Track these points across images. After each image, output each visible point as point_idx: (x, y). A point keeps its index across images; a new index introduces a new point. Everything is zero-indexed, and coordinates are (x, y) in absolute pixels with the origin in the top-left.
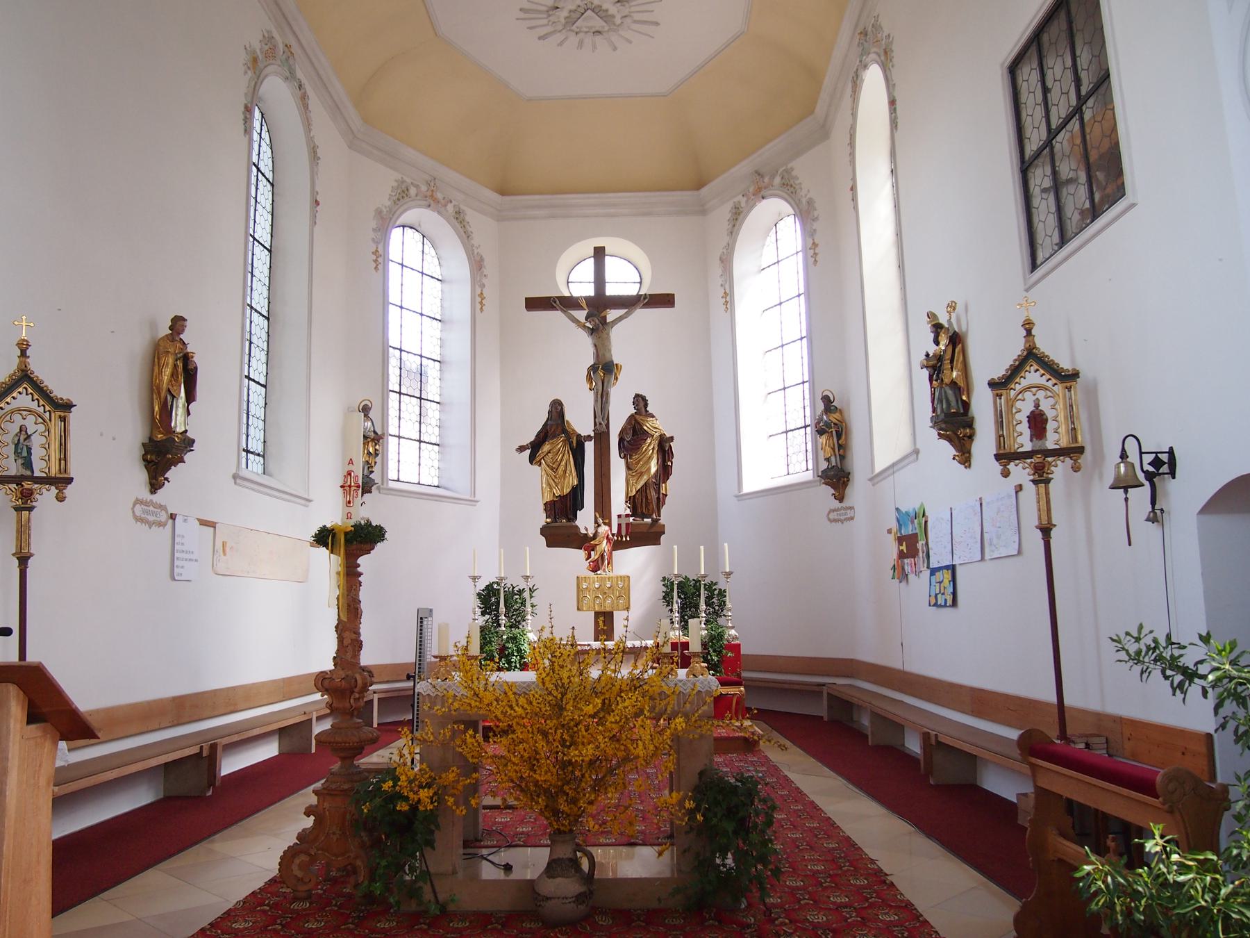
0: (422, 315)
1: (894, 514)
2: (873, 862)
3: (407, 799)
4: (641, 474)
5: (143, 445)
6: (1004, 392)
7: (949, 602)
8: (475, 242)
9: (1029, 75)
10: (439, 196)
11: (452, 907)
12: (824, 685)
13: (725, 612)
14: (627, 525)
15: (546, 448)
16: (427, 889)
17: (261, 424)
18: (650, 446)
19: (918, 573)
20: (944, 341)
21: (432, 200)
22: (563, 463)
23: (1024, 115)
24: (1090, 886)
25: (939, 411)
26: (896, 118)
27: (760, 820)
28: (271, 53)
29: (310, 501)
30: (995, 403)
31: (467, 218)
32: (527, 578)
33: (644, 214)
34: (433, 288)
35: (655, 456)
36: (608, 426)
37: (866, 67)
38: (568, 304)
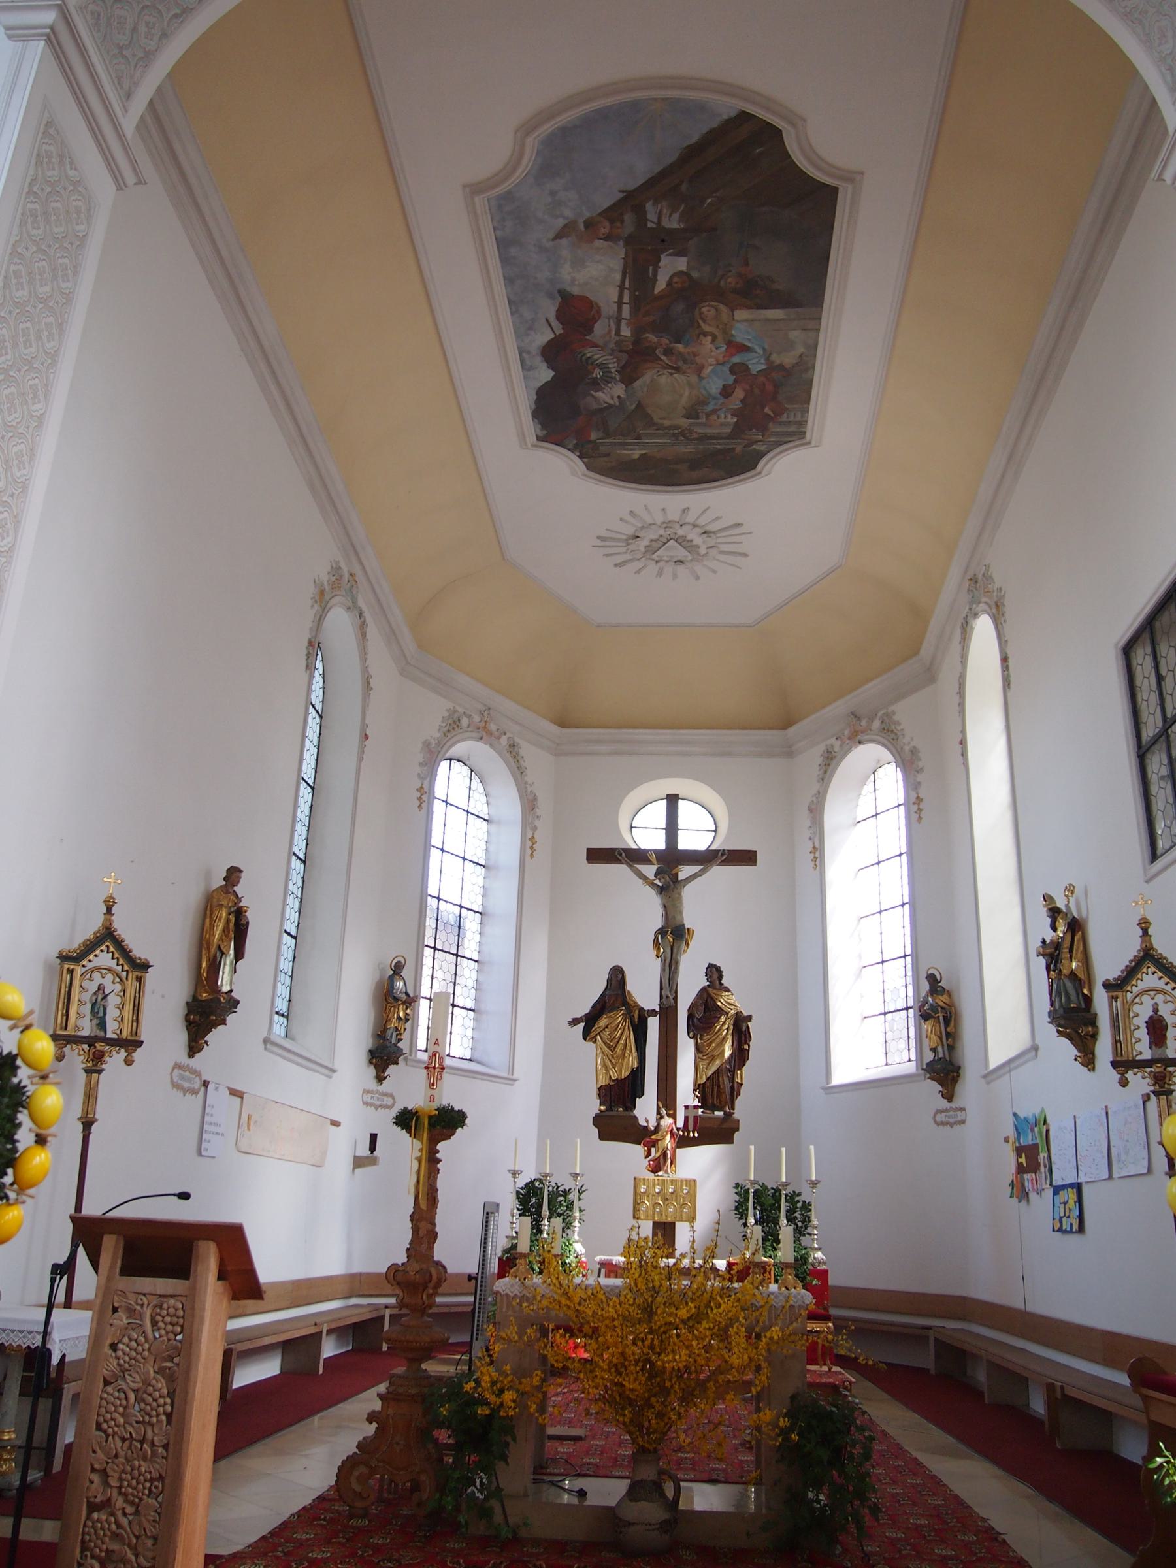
0: (464, 859)
1: (1011, 1120)
2: (983, 1520)
3: (488, 1404)
4: (713, 1058)
5: (187, 1003)
6: (1120, 994)
7: (1075, 1227)
8: (529, 779)
9: (1142, 659)
10: (493, 727)
11: (523, 1533)
12: (929, 1328)
13: (809, 1230)
14: (696, 1118)
15: (603, 1022)
16: (498, 1509)
17: (288, 979)
18: (724, 1026)
19: (1040, 1192)
20: (1062, 928)
21: (484, 732)
22: (622, 1041)
23: (1139, 699)
24: (1163, 1479)
25: (1057, 1005)
26: (1008, 675)
27: (857, 1451)
28: (336, 585)
29: (333, 1071)
30: (1111, 1006)
31: (522, 752)
32: (575, 1176)
33: (723, 754)
34: (479, 829)
35: (730, 1037)
36: (675, 999)
37: (976, 615)
38: (635, 857)
